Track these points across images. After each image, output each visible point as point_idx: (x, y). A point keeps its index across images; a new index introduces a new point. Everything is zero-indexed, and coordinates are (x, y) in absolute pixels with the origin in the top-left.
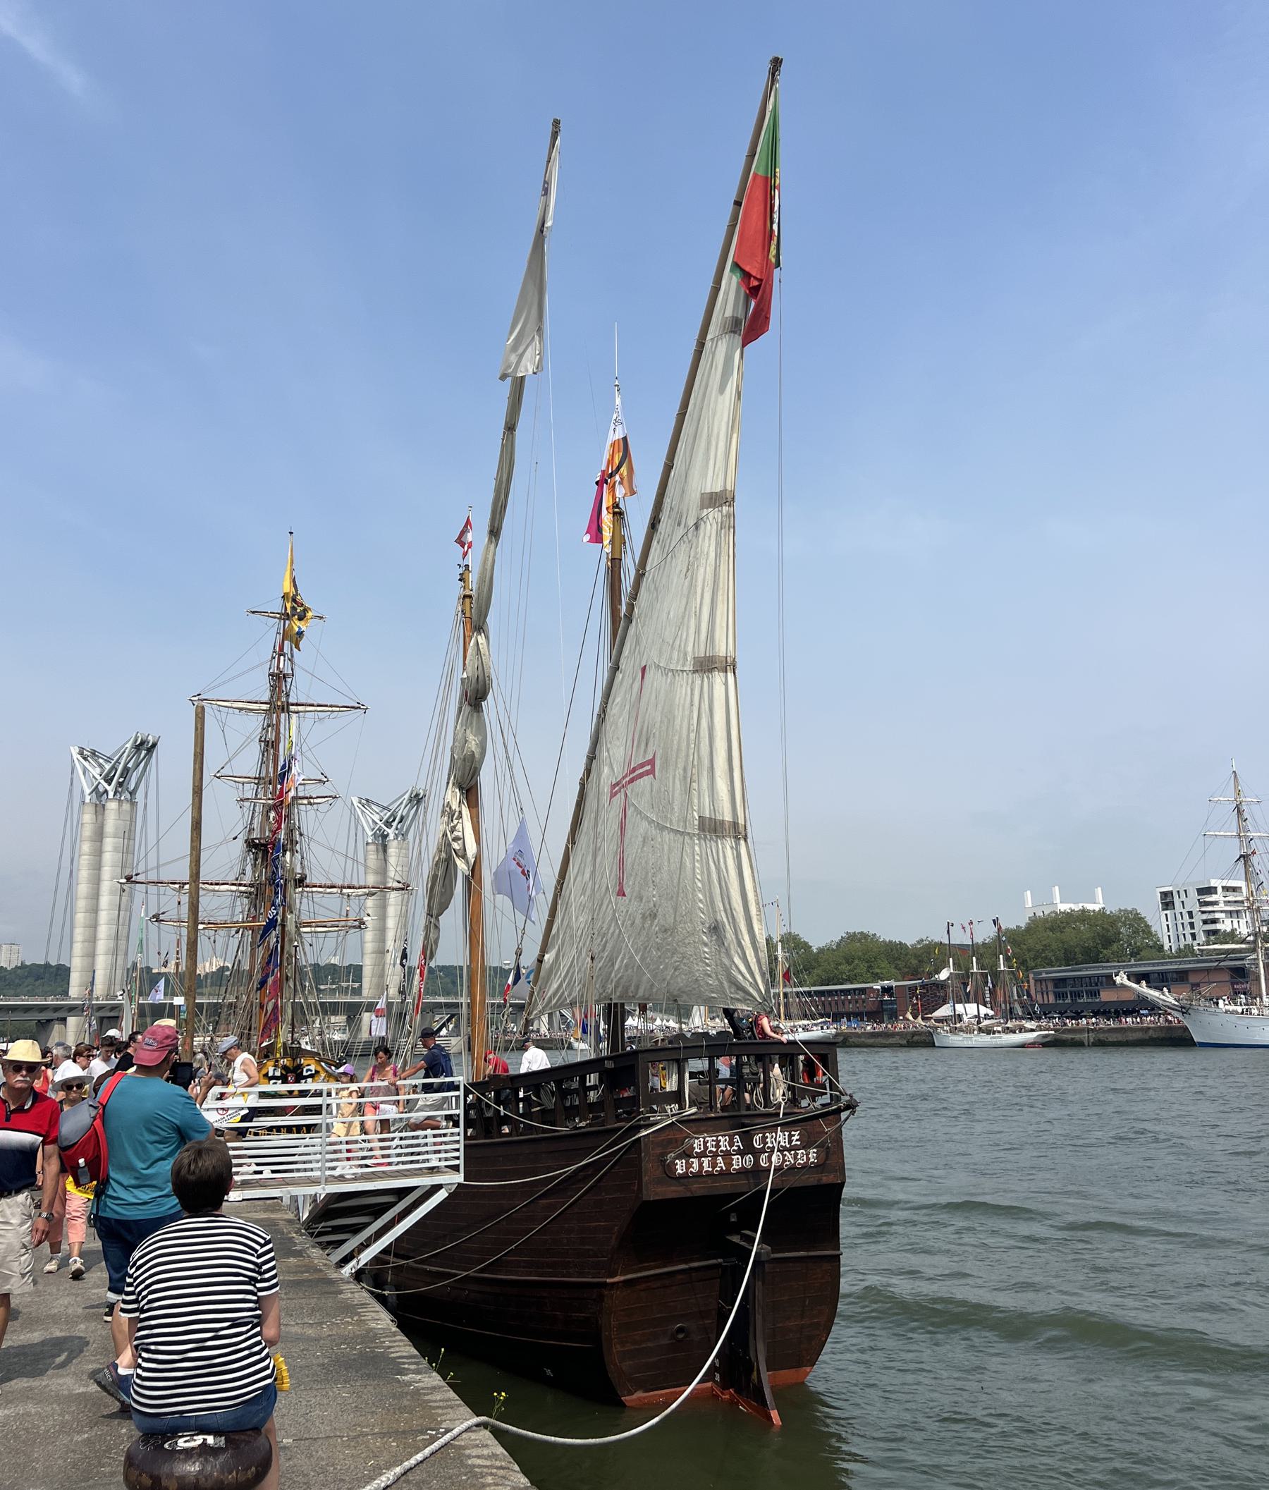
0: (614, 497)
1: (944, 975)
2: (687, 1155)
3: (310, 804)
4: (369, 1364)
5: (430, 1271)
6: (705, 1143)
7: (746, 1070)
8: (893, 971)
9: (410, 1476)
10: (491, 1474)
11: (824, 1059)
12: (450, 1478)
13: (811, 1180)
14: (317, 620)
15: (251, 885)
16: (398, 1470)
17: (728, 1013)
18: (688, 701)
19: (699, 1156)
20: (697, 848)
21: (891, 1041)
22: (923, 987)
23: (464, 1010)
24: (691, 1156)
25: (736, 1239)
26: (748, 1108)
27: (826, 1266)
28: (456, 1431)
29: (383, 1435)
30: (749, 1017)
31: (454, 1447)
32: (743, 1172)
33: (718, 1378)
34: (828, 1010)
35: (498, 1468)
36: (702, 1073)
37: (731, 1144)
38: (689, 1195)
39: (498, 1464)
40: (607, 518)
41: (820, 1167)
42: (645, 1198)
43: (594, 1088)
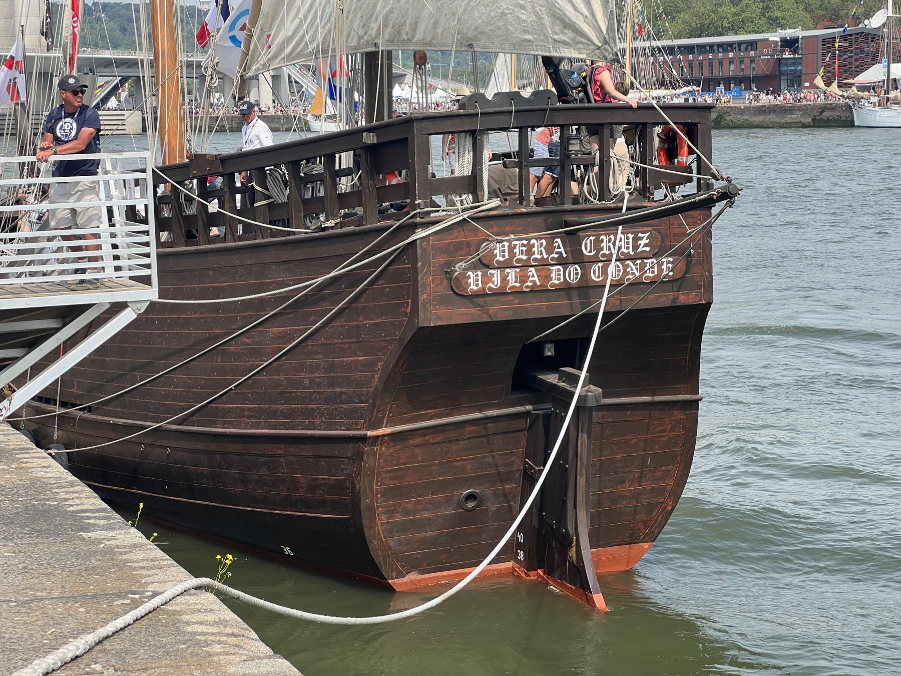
1: (876, 21)
2: (484, 265)
4: (43, 519)
5: (114, 424)
6: (511, 249)
7: (574, 147)
8: (801, 13)
9: (107, 645)
10: (220, 642)
11: (691, 130)
12: (163, 647)
13: (663, 299)
16: (91, 638)
17: (550, 63)
19: (503, 266)
21: (788, 118)
22: (844, 38)
23: (146, 72)
24: (488, 267)
25: (552, 378)
26: (576, 200)
27: (678, 415)
28: (168, 595)
29: (64, 599)
30: (581, 70)
31: (166, 612)
32: (566, 289)
33: (521, 555)
34: (697, 74)
35: (227, 635)
36: (507, 155)
37: (550, 249)
38: (485, 319)
39: (228, 630)
41: (677, 282)
42: (422, 324)
43: (348, 172)
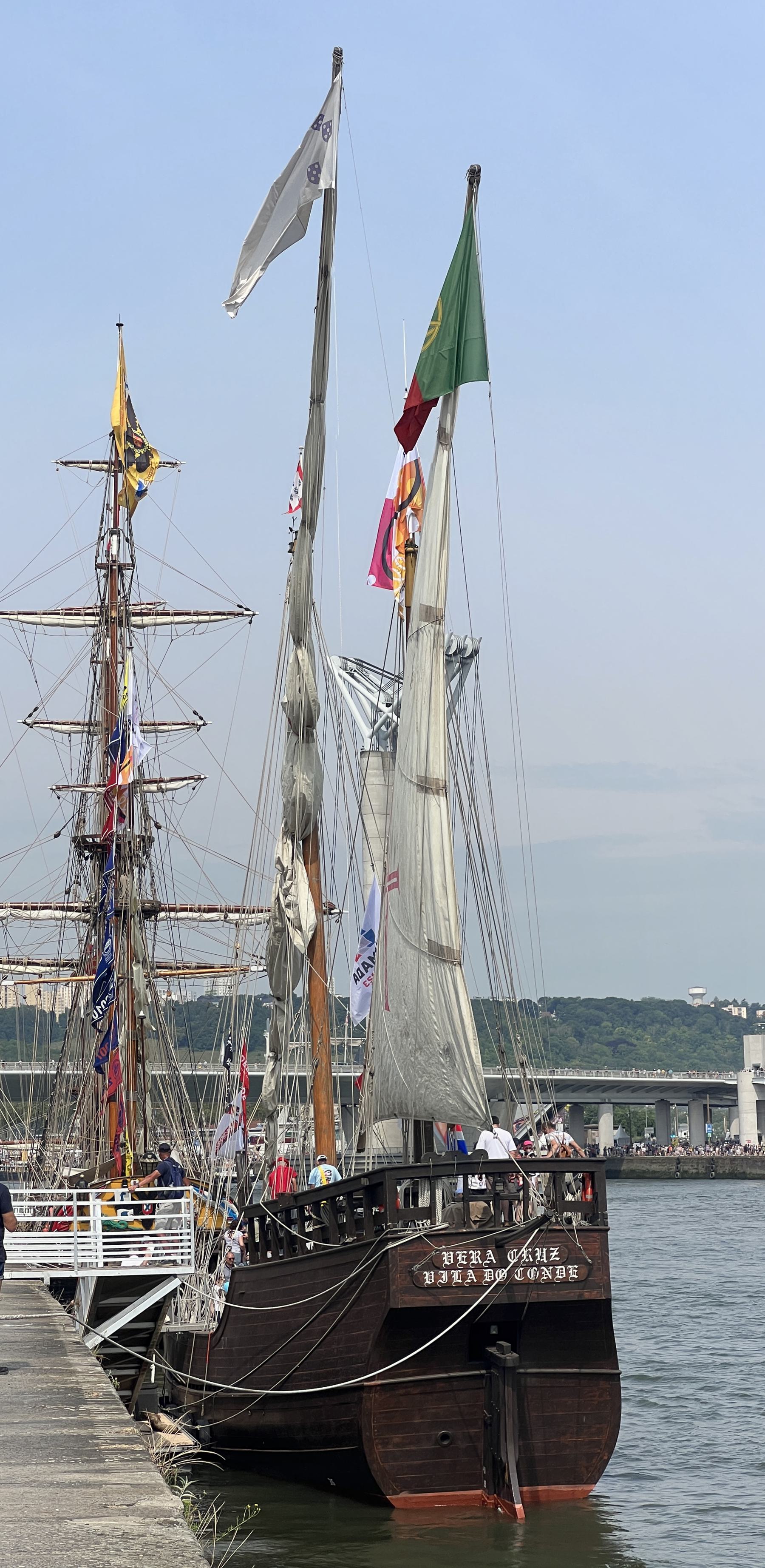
0: (407, 533)
3: (161, 790)
6: (455, 1257)
13: (572, 1295)
14: (168, 469)
15: (86, 910)
18: (414, 821)
19: (449, 1268)
20: (429, 971)
24: (439, 1269)
27: (603, 1384)
37: (484, 1257)
38: (437, 1305)
40: (397, 559)
